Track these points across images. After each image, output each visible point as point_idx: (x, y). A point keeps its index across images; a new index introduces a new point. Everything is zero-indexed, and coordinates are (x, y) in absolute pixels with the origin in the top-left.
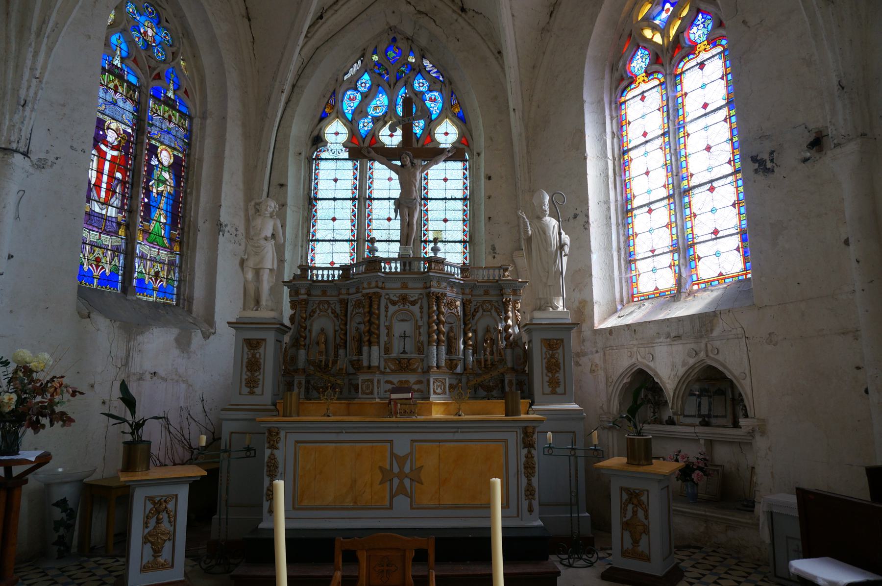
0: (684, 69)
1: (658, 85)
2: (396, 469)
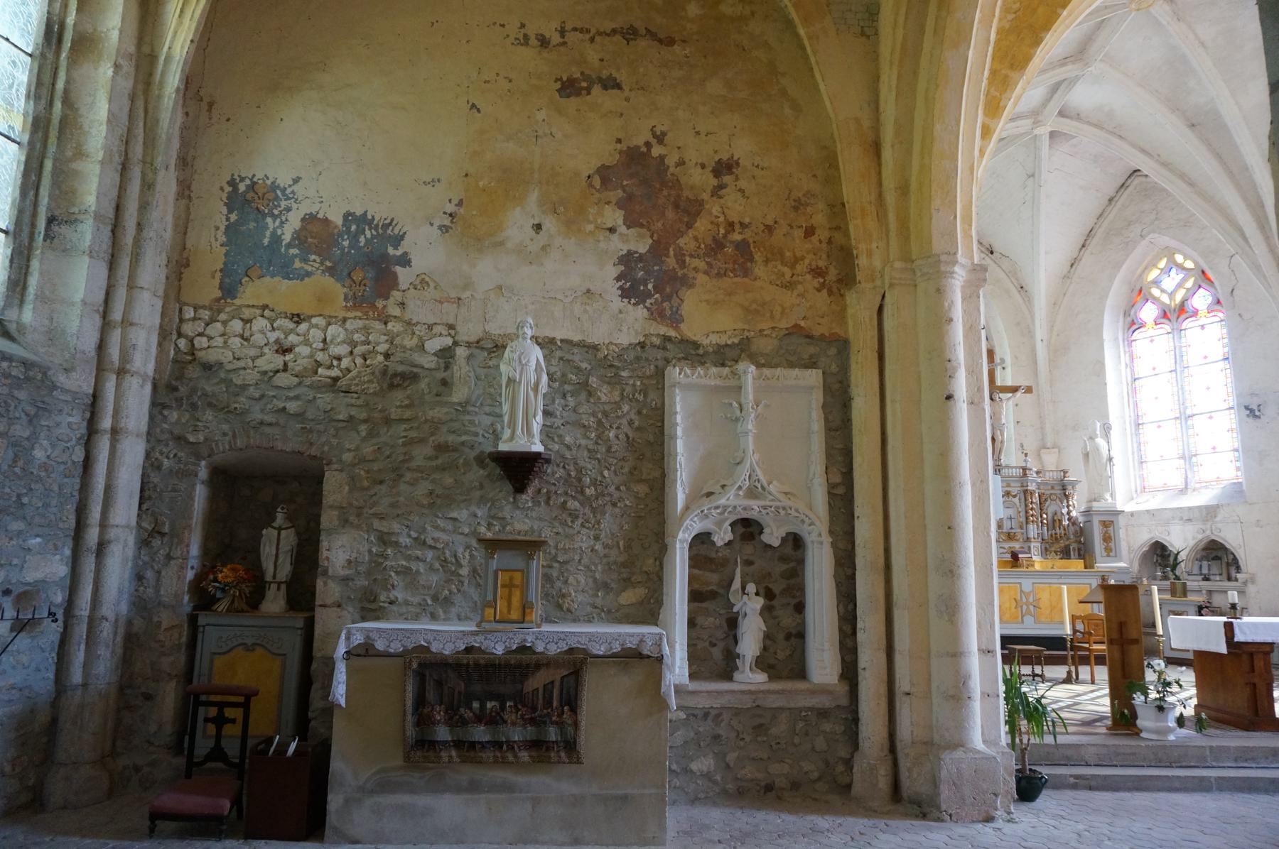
2: (1024, 600)
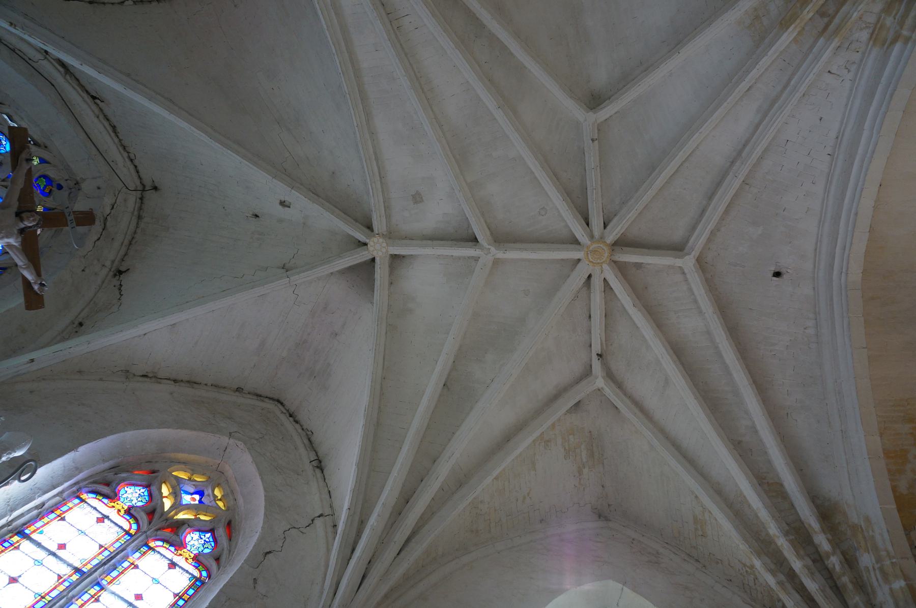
0: (157, 549)
1: (124, 530)
